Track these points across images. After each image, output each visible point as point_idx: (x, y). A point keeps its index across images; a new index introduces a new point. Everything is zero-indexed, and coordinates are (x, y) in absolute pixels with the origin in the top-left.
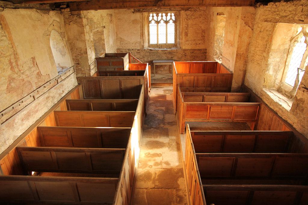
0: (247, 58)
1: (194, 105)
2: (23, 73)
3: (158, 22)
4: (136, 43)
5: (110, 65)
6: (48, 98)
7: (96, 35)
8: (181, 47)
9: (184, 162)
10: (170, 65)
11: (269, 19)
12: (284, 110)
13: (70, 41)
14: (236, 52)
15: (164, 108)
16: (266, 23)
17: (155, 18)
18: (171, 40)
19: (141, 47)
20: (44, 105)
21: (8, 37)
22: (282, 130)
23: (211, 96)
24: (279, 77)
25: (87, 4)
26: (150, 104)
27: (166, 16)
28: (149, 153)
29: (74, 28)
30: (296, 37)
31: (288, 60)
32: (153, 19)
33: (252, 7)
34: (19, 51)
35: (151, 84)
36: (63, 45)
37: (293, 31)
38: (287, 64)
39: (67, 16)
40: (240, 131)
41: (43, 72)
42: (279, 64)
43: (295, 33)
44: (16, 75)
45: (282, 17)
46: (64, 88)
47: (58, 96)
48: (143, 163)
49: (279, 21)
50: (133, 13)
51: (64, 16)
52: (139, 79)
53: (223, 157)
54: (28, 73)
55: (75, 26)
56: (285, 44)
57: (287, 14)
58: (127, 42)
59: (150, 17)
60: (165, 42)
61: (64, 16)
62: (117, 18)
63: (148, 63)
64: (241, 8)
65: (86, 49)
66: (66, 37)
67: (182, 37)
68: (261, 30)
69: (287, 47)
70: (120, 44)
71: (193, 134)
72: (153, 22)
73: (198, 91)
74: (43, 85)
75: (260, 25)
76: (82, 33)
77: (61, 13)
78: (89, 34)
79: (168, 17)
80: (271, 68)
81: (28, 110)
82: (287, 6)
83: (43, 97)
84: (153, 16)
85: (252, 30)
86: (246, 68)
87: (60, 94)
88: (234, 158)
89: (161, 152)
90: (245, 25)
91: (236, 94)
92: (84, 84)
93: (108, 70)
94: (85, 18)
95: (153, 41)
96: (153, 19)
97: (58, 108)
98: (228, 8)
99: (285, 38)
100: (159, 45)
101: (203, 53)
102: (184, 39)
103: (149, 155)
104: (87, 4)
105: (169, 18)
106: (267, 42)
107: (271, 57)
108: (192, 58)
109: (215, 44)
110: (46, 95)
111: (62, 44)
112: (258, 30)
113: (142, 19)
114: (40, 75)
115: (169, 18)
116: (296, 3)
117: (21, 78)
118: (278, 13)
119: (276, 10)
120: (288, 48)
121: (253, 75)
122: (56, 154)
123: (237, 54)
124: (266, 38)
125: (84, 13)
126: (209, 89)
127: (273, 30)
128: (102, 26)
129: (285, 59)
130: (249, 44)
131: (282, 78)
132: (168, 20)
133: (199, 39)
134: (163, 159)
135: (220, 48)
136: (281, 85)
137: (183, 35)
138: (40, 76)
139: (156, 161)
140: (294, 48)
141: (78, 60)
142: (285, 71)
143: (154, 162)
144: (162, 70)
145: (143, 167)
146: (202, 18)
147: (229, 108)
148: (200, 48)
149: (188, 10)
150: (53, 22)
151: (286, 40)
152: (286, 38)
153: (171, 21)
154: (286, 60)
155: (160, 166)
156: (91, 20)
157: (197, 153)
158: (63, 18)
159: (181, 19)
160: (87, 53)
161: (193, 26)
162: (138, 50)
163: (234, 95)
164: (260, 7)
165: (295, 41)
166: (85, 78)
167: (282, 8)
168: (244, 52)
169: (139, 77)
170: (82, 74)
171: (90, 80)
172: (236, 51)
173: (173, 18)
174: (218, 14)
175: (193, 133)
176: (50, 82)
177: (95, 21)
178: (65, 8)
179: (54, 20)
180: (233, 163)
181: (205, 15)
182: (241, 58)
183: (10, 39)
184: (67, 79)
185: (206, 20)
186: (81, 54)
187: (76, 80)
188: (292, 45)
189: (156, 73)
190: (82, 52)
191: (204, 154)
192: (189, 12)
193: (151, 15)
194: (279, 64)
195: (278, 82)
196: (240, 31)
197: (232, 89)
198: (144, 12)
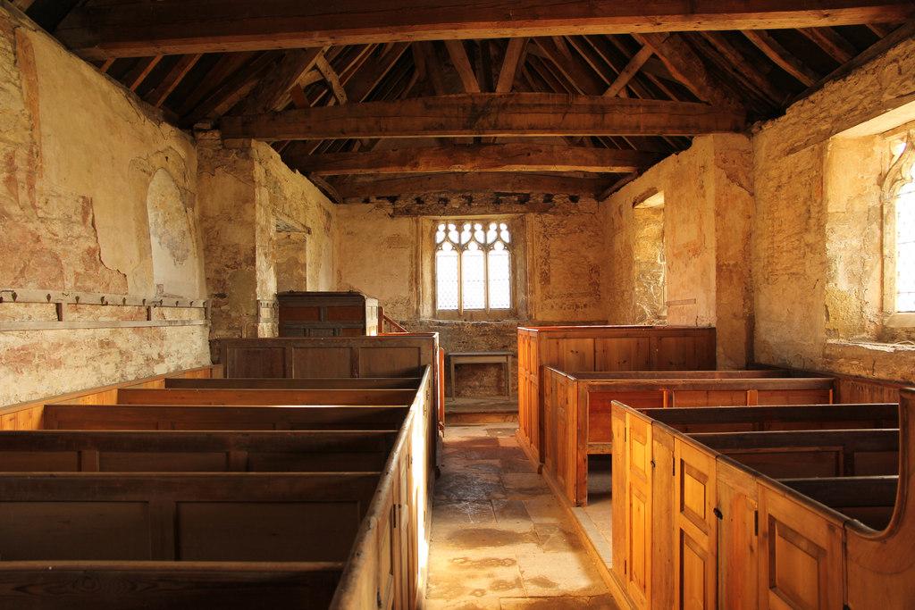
0: (750, 276)
1: (614, 390)
2: (42, 220)
3: (460, 248)
5: (320, 320)
7: (282, 248)
8: (530, 317)
9: (610, 571)
11: (799, 144)
13: (205, 224)
14: (713, 262)
15: (496, 462)
17: (454, 235)
18: (501, 299)
21: (25, 93)
24: (872, 295)
25: (274, 120)
26: (449, 455)
27: (485, 229)
28: (466, 560)
29: (225, 186)
31: (887, 240)
32: (447, 239)
33: (741, 135)
34: (49, 151)
35: (445, 414)
36: (185, 227)
37: (879, 157)
38: (886, 252)
39: (209, 152)
41: (106, 255)
42: (863, 254)
43: (888, 160)
44: (18, 208)
45: (838, 119)
47: (141, 360)
48: (447, 584)
50: (392, 216)
52: (415, 345)
54: (58, 228)
55: (229, 178)
57: (853, 104)
60: (481, 306)
64: (710, 137)
65: (255, 247)
66: (197, 208)
67: (534, 287)
69: (873, 201)
72: (447, 246)
75: (773, 173)
76: (249, 200)
77: (195, 141)
79: (489, 233)
81: (28, 342)
82: (846, 86)
84: (445, 232)
85: (752, 194)
86: (751, 309)
89: (512, 556)
90: (727, 181)
92: (233, 362)
95: (447, 302)
96: (447, 239)
100: (466, 312)
102: (538, 291)
103: (468, 564)
104: (274, 120)
105: (492, 235)
107: (832, 237)
109: (637, 289)
111: (181, 224)
113: (415, 233)
115: (492, 235)
116: (874, 67)
117: (31, 226)
118: (822, 115)
119: (817, 110)
120: (879, 206)
121: (783, 319)
122: (101, 458)
123: (717, 264)
124: (804, 193)
129: (877, 240)
130: (749, 236)
131: (882, 300)
132: (489, 242)
134: (522, 572)
135: (651, 298)
136: (886, 320)
137: (537, 279)
139: (496, 579)
140: (898, 203)
141: (224, 283)
142: (887, 275)
143: (491, 580)
144: (475, 387)
145: (448, 596)
149: (546, 211)
152: (865, 178)
153: (499, 246)
154: (882, 241)
155: (516, 592)
158: (195, 156)
159: (528, 237)
160: (253, 261)
165: (894, 182)
166: (239, 342)
170: (229, 329)
171: (255, 346)
172: (714, 256)
173: (506, 236)
178: (205, 131)
182: (731, 278)
183: (31, 104)
186: (237, 265)
187: (208, 347)
188: (887, 195)
189: (458, 394)
190: (240, 258)
192: (548, 218)
193: (442, 227)
194: (863, 254)
195: (871, 311)
196: (718, 200)
198: (423, 214)
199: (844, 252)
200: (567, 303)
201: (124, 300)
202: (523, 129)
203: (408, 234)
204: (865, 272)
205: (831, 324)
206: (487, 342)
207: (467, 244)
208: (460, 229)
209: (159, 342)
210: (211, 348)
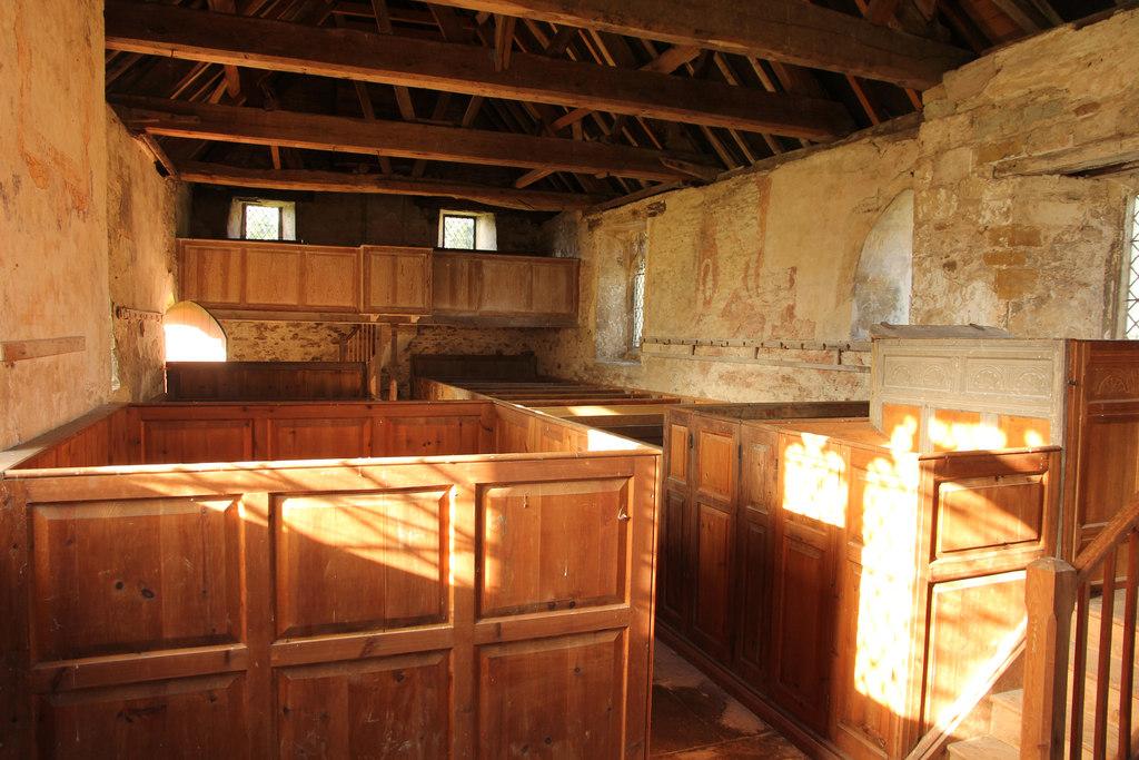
41: (798, 312)
201: (802, 345)
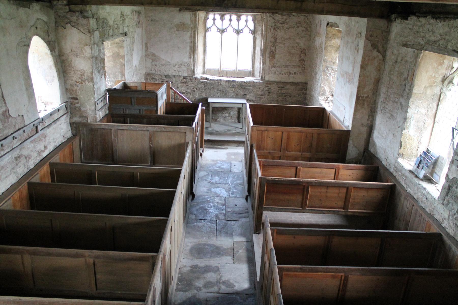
4: (181, 65)
5: (131, 104)
6: (18, 158)
10: (277, 233)
12: (429, 197)
16: (405, 48)
19: (190, 73)
20: (11, 170)
22: (425, 231)
23: (309, 169)
27: (238, 19)
30: (451, 76)
40: (355, 230)
41: (13, 113)
45: (428, 42)
46: (47, 140)
47: (36, 155)
49: (425, 48)
51: (57, 12)
53: (323, 273)
55: (74, 30)
56: (435, 85)
58: (164, 62)
59: (208, 21)
61: (57, 12)
62: (148, 18)
63: (200, 104)
68: (397, 59)
70: (152, 65)
71: (275, 232)
72: (214, 29)
73: (288, 158)
74: (12, 134)
75: (395, 52)
78: (97, 45)
80: (411, 125)
83: (10, 156)
87: (39, 153)
88: (342, 276)
90: (371, 48)
91: (354, 166)
93: (128, 112)
94: (93, 17)
95: (212, 64)
97: (35, 178)
98: (345, 19)
99: (435, 76)
100: (223, 71)
101: (302, 90)
106: (406, 81)
108: (281, 98)
110: (16, 153)
112: (393, 59)
113: (193, 22)
114: (7, 116)
120: (439, 93)
124: (405, 75)
125: (92, 6)
126: (308, 155)
127: (416, 62)
128: (121, 31)
132: (240, 28)
133: (294, 64)
138: (8, 118)
146: (300, 29)
147: (339, 190)
148: (296, 81)
150: (36, 22)
151: (436, 80)
152: (436, 77)
153: (246, 31)
156: (103, 22)
157: (281, 266)
161: (286, 41)
162: (184, 78)
163: (350, 168)
164: (395, 20)
167: (427, 27)
168: (370, 95)
169: (183, 128)
173: (251, 25)
174: (328, 24)
175: (276, 230)
176: (24, 129)
177: (111, 23)
179: (38, 19)
180: (340, 283)
181: (307, 24)
182: (364, 104)
184: (54, 126)
185: (309, 33)
191: (291, 268)
197: (348, 158)
199: (416, 115)
200: (285, 71)
202: (252, 8)
203: (189, 23)
204: (424, 128)
205: (401, 151)
206: (234, 92)
207: (226, 29)
208: (222, 18)
209: (43, 139)
210: (71, 127)
